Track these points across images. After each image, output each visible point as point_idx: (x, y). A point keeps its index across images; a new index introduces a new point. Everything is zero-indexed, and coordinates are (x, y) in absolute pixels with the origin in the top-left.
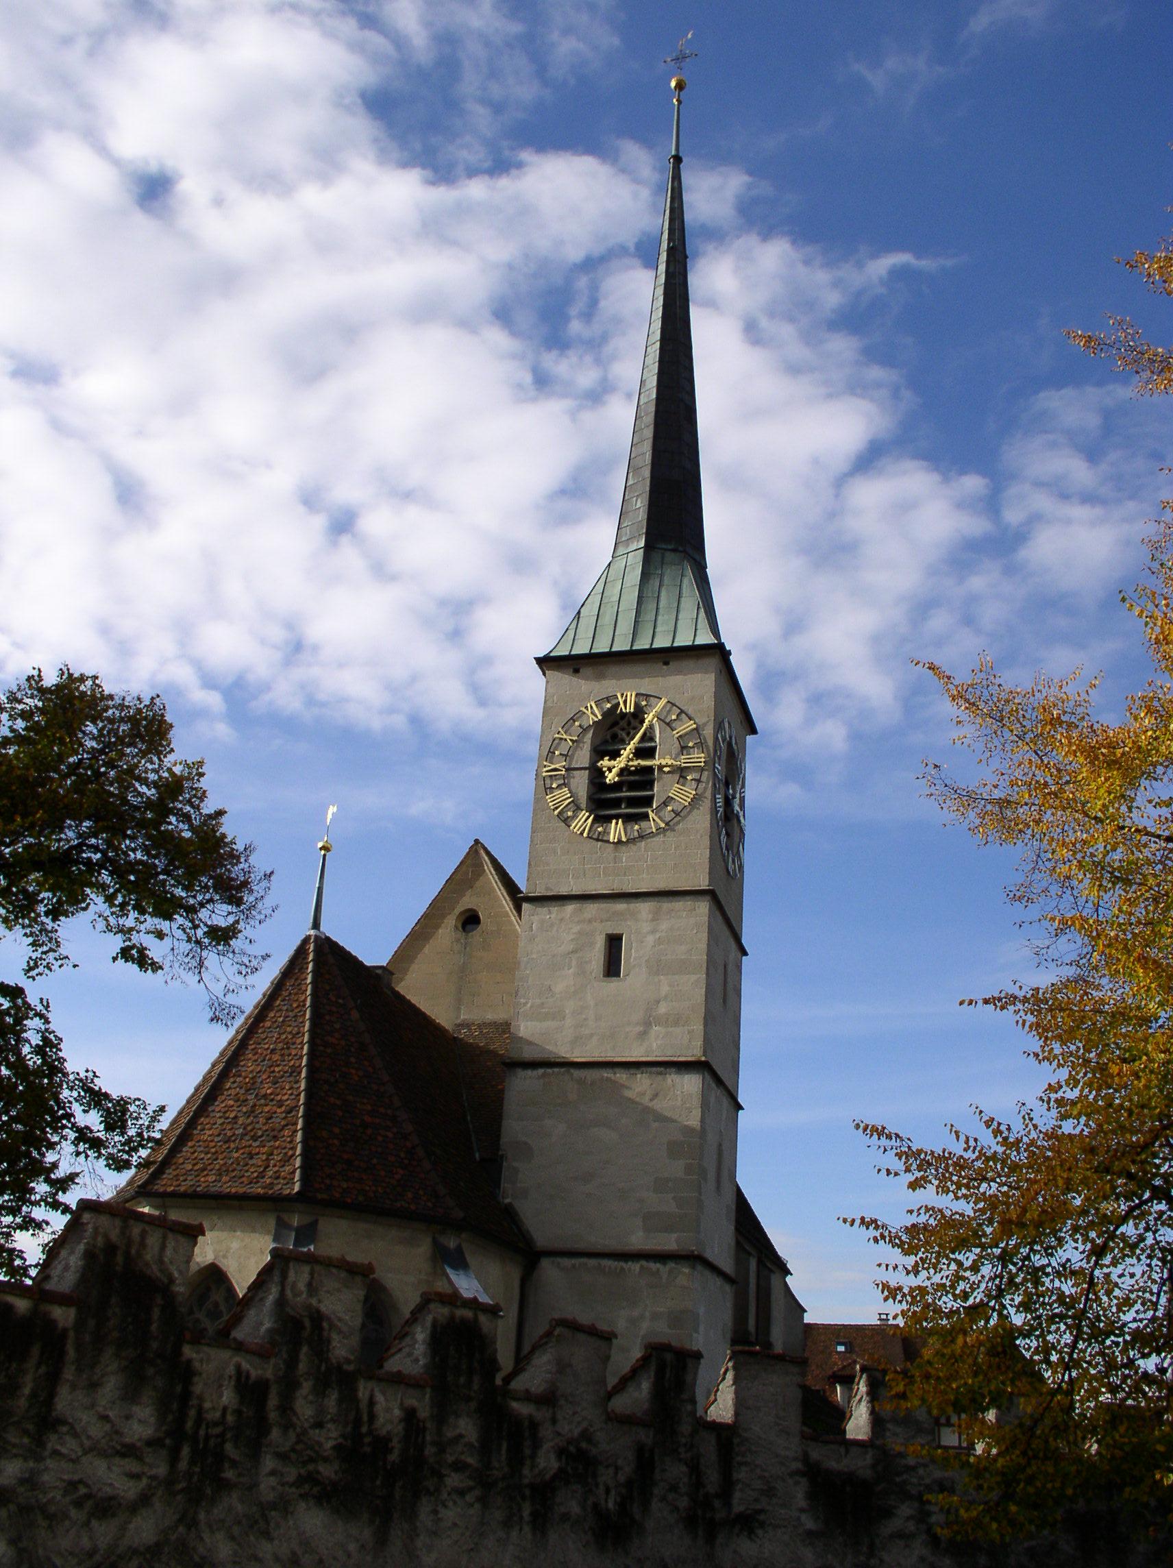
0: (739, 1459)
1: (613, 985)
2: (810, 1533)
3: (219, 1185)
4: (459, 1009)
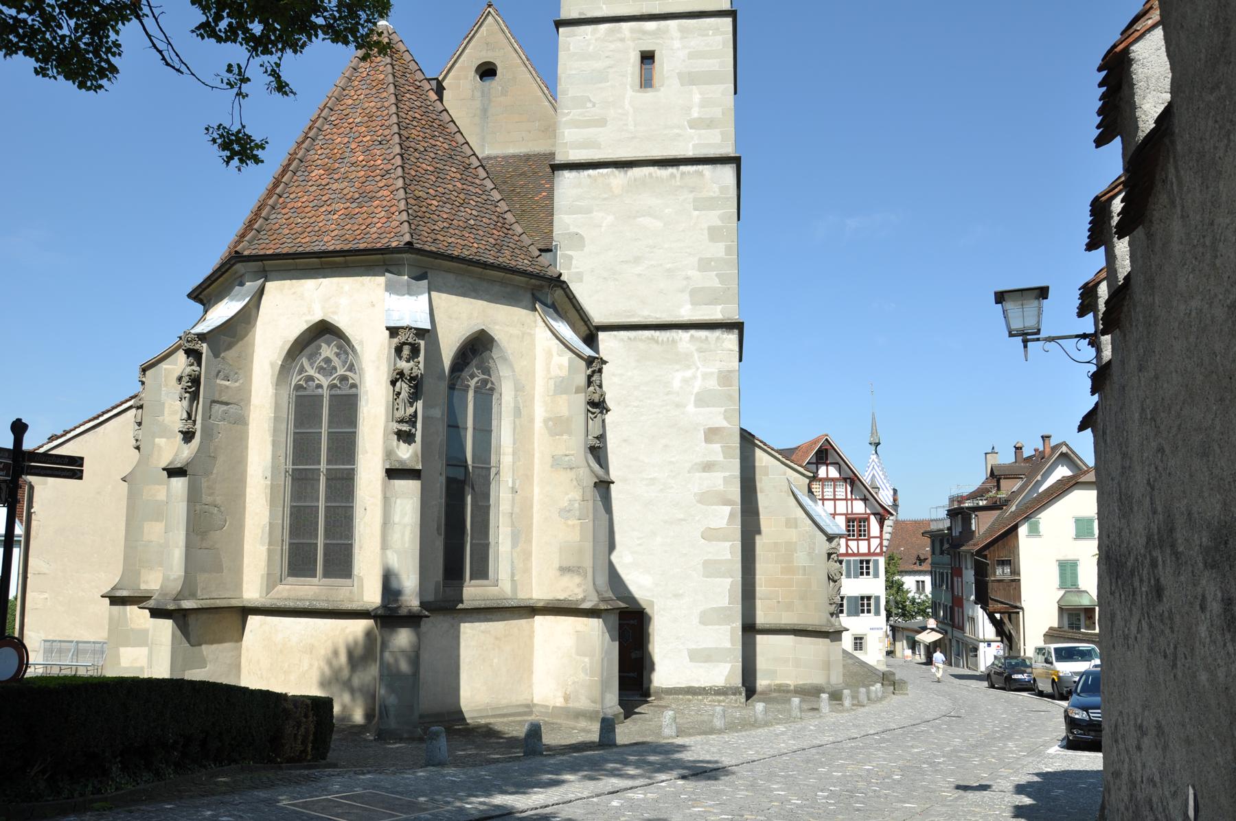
1: (649, 95)
3: (322, 243)
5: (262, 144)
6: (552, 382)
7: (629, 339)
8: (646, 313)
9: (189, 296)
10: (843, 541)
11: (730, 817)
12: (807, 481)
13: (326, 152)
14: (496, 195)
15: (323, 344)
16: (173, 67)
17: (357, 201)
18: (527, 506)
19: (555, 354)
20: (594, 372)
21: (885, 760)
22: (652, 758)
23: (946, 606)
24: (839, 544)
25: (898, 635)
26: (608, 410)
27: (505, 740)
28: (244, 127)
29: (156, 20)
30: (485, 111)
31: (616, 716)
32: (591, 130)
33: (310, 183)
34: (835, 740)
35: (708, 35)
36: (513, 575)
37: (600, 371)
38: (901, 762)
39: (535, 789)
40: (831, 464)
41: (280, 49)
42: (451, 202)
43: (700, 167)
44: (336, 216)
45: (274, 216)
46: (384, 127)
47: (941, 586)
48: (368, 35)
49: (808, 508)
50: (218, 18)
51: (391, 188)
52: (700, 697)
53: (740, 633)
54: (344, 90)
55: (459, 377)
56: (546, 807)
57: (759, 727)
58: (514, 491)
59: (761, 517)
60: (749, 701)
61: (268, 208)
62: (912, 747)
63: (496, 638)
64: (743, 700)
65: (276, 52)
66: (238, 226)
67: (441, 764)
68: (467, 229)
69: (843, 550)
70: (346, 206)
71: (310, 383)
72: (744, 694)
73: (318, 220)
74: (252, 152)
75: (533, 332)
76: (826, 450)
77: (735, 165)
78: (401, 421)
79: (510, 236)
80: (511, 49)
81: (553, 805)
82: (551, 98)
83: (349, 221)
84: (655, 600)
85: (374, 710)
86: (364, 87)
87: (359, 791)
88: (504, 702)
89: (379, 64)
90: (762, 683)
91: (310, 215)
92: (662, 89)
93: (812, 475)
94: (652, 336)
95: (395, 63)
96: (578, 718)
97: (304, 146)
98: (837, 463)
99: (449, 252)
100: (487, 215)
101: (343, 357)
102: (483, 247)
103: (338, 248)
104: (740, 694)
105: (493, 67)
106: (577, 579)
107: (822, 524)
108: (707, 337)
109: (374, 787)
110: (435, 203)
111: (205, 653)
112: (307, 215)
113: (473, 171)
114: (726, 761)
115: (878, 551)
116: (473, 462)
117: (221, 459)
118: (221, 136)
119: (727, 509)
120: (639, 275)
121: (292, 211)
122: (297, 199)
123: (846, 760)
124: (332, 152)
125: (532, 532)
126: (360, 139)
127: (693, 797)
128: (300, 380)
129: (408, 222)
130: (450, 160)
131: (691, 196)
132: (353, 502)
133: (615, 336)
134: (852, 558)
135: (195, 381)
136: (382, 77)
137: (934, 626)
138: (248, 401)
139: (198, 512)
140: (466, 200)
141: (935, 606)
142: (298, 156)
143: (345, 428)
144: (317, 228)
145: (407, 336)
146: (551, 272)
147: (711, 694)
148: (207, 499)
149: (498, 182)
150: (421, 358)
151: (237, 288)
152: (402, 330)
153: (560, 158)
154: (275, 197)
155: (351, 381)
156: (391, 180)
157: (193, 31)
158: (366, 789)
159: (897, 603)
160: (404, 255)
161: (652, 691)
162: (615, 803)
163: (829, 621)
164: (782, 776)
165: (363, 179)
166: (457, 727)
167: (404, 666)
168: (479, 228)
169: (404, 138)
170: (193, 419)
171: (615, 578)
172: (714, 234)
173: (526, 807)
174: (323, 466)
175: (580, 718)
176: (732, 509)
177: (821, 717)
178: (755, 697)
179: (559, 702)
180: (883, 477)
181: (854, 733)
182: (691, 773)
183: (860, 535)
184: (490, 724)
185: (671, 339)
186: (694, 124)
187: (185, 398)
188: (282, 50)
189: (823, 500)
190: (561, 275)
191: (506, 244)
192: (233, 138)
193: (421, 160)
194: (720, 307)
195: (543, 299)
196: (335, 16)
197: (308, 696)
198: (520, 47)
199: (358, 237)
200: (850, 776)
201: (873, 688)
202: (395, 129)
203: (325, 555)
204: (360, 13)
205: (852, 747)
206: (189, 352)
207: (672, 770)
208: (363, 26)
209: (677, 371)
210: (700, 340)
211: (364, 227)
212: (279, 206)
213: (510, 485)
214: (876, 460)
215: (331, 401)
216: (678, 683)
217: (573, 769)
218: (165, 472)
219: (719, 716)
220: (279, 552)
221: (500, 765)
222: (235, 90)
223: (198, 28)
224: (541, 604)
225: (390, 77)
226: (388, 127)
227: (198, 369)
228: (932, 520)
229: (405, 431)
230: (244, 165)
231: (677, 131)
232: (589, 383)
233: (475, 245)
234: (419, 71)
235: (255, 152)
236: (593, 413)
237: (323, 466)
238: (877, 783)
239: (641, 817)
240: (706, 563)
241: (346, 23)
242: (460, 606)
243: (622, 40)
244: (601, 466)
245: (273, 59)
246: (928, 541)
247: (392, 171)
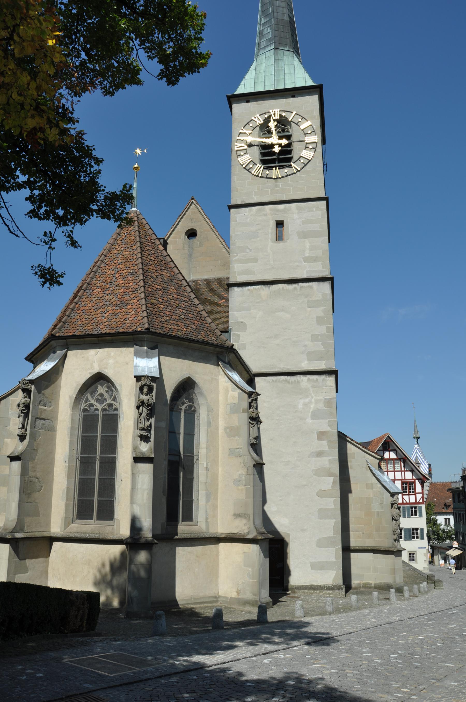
1: (281, 245)
5: (62, 275)
6: (229, 406)
7: (273, 381)
8: (282, 366)
9: (26, 359)
10: (400, 496)
11: (337, 671)
12: (378, 461)
13: (102, 279)
14: (196, 302)
15: (99, 386)
16: (14, 234)
17: (119, 306)
18: (215, 478)
19: (230, 390)
20: (252, 400)
21: (431, 633)
22: (289, 631)
23: (464, 533)
24: (398, 498)
25: (436, 551)
26: (261, 422)
27: (201, 619)
28: (52, 265)
29: (7, 209)
30: (190, 255)
31: (267, 603)
32: (250, 264)
33: (93, 296)
34: (400, 619)
35: (313, 211)
36: (207, 519)
37: (256, 400)
38: (441, 634)
39: (218, 652)
40: (392, 450)
41: (73, 223)
42: (171, 306)
43: (311, 284)
44: (107, 314)
45: (73, 314)
46: (134, 265)
47: (460, 521)
48: (120, 215)
49: (379, 477)
50: (40, 207)
52: (318, 591)
53: (341, 552)
54: (112, 245)
55: (175, 404)
56: (224, 663)
57: (354, 610)
58: (207, 469)
59: (351, 483)
60: (347, 594)
61: (70, 310)
62: (448, 624)
63: (197, 556)
64: (344, 593)
65: (71, 224)
66: (54, 320)
67: (163, 635)
68: (180, 320)
69: (400, 501)
70: (112, 308)
71: (92, 408)
72: (344, 590)
73: (97, 316)
74: (56, 279)
75: (217, 378)
76: (389, 442)
77: (330, 282)
78: (142, 430)
79: (204, 324)
80: (204, 221)
81: (228, 662)
82: (227, 248)
83: (114, 317)
84: (290, 533)
85: (125, 599)
86: (123, 244)
87: (112, 652)
88: (201, 595)
89: (132, 231)
90: (355, 582)
91: (93, 314)
92: (288, 241)
93: (380, 457)
94: (286, 379)
95: (140, 230)
96: (245, 605)
97: (90, 276)
98: (395, 450)
99: (170, 333)
100: (191, 313)
101: (110, 393)
102: (189, 331)
103: (108, 332)
104: (342, 589)
105: (195, 231)
106: (244, 521)
107: (387, 486)
108: (317, 379)
109: (121, 650)
110: (162, 306)
111: (27, 564)
112: (91, 314)
113: (183, 288)
114: (334, 633)
115: (421, 501)
116: (184, 453)
117: (40, 451)
118: (40, 271)
119: (332, 479)
120: (278, 345)
121: (83, 311)
122: (86, 305)
123: (407, 632)
124: (105, 279)
125: (218, 493)
126: (121, 272)
127: (314, 657)
128: (86, 406)
129: (147, 317)
130: (171, 282)
132: (115, 476)
133: (265, 379)
134: (406, 506)
135: (27, 406)
136: (133, 238)
137: (457, 546)
138: (57, 418)
139: (26, 481)
140: (179, 305)
141: (457, 533)
142: (87, 282)
143: (111, 433)
144: (96, 321)
145: (146, 381)
146: (228, 344)
147: (324, 590)
148: (31, 474)
149: (198, 294)
150: (154, 394)
151: (52, 354)
152: (143, 378)
153: (232, 281)
154: (74, 304)
155: (114, 407)
156: (138, 294)
157: (26, 215)
158: (115, 651)
159: (434, 532)
160: (145, 336)
161: (289, 587)
162: (266, 661)
163: (393, 544)
164: (369, 643)
165: (123, 294)
166: (173, 610)
167: (143, 573)
168: (187, 320)
169: (145, 271)
170: (25, 428)
171: (266, 520)
172: (320, 320)
173: (212, 664)
174: (98, 455)
175: (247, 605)
176: (334, 478)
177: (391, 604)
178: (351, 591)
179: (234, 595)
180: (422, 457)
181: (411, 614)
182: (313, 641)
183: (410, 492)
184: (193, 608)
185: (296, 381)
187: (21, 416)
188: (74, 223)
189: (388, 471)
190: (233, 345)
191: (202, 329)
192: (47, 271)
193: (154, 283)
194: (324, 362)
196: (103, 204)
197: (85, 591)
198: (210, 220)
199: (119, 326)
200: (411, 643)
201: (422, 585)
202: (140, 266)
203: (98, 506)
204: (117, 202)
205: (411, 624)
206: (24, 390)
207: (301, 639)
208: (118, 209)
209: (301, 399)
211: (123, 320)
212: (76, 309)
213: (205, 466)
214: (418, 448)
215: (102, 418)
216: (305, 583)
217: (241, 638)
218: (9, 458)
219: (329, 604)
220: (72, 504)
221: (197, 635)
222: (48, 246)
223: (29, 213)
224: (223, 536)
225: (138, 238)
226: (136, 265)
227: (29, 400)
228: (452, 482)
229: (145, 435)
230: (52, 286)
231: (297, 264)
232: (250, 407)
233: (185, 329)
234: (153, 235)
235: (58, 279)
236: (252, 424)
237: (98, 455)
238: (427, 649)
239: (282, 671)
240: (320, 511)
241: (109, 208)
242: (176, 537)
243: (266, 215)
244: (257, 455)
245: (69, 228)
246: (450, 494)
247: (139, 289)
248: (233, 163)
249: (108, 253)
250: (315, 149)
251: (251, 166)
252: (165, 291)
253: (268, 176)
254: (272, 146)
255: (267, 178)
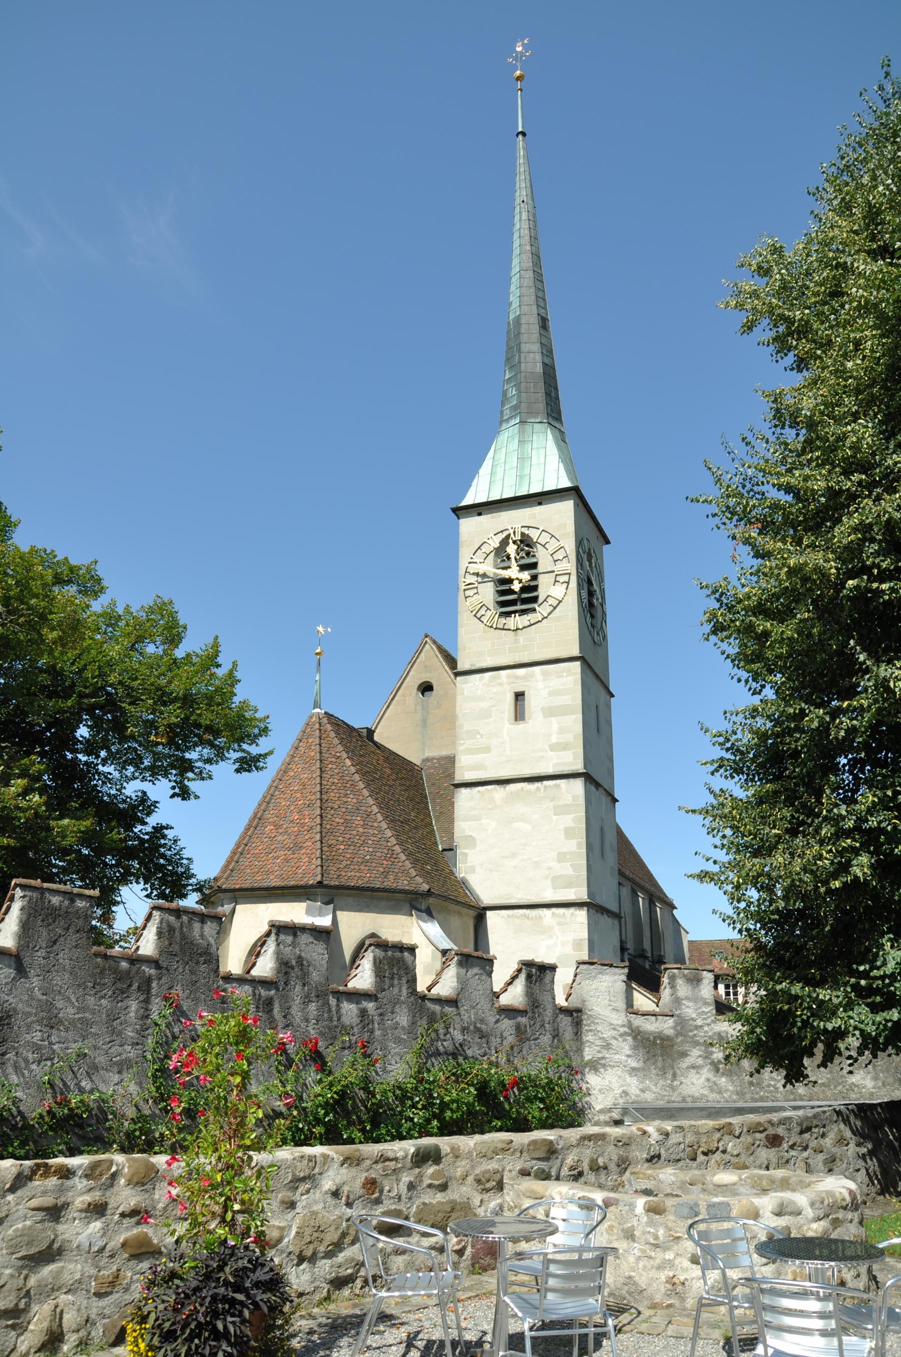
0: (586, 1028)
1: (521, 726)
2: (634, 1069)
4: (424, 750)
30: (424, 721)
35: (562, 677)
43: (558, 782)
51: (313, 840)
110: (342, 847)
120: (515, 867)
131: (552, 804)
165: (296, 833)
172: (569, 833)
186: (554, 748)
195: (418, 906)
210: (559, 916)
231: (541, 754)
243: (501, 684)
248: (460, 609)
249: (283, 776)
250: (568, 583)
251: (483, 613)
252: (349, 825)
253: (506, 627)
254: (510, 581)
255: (503, 629)
